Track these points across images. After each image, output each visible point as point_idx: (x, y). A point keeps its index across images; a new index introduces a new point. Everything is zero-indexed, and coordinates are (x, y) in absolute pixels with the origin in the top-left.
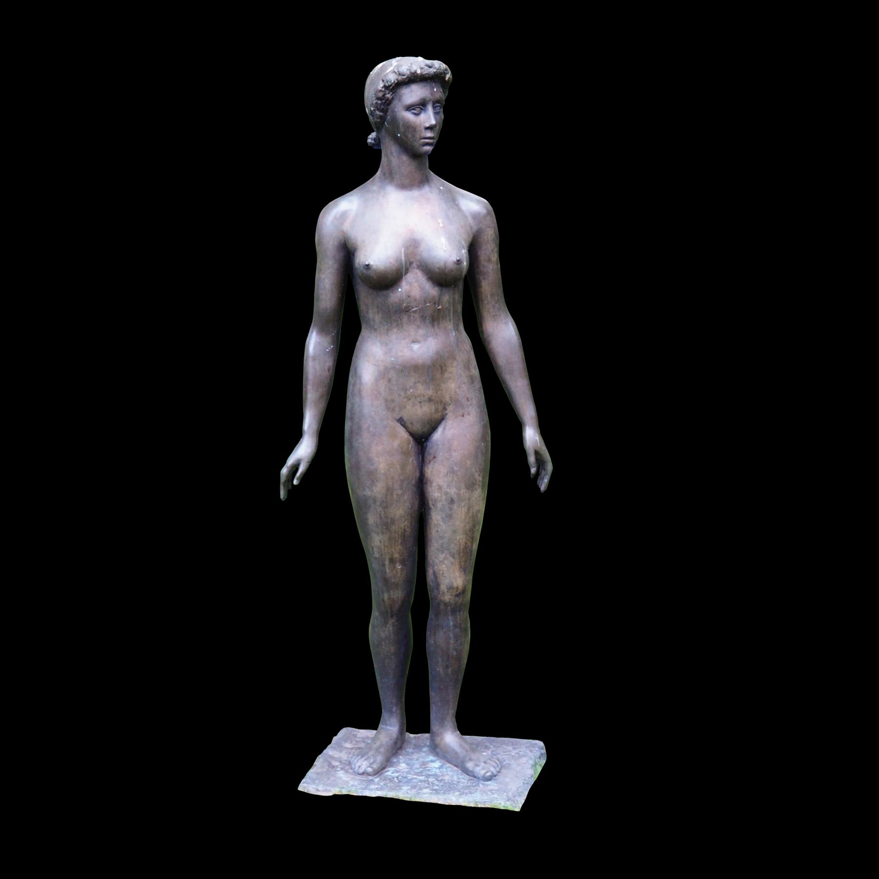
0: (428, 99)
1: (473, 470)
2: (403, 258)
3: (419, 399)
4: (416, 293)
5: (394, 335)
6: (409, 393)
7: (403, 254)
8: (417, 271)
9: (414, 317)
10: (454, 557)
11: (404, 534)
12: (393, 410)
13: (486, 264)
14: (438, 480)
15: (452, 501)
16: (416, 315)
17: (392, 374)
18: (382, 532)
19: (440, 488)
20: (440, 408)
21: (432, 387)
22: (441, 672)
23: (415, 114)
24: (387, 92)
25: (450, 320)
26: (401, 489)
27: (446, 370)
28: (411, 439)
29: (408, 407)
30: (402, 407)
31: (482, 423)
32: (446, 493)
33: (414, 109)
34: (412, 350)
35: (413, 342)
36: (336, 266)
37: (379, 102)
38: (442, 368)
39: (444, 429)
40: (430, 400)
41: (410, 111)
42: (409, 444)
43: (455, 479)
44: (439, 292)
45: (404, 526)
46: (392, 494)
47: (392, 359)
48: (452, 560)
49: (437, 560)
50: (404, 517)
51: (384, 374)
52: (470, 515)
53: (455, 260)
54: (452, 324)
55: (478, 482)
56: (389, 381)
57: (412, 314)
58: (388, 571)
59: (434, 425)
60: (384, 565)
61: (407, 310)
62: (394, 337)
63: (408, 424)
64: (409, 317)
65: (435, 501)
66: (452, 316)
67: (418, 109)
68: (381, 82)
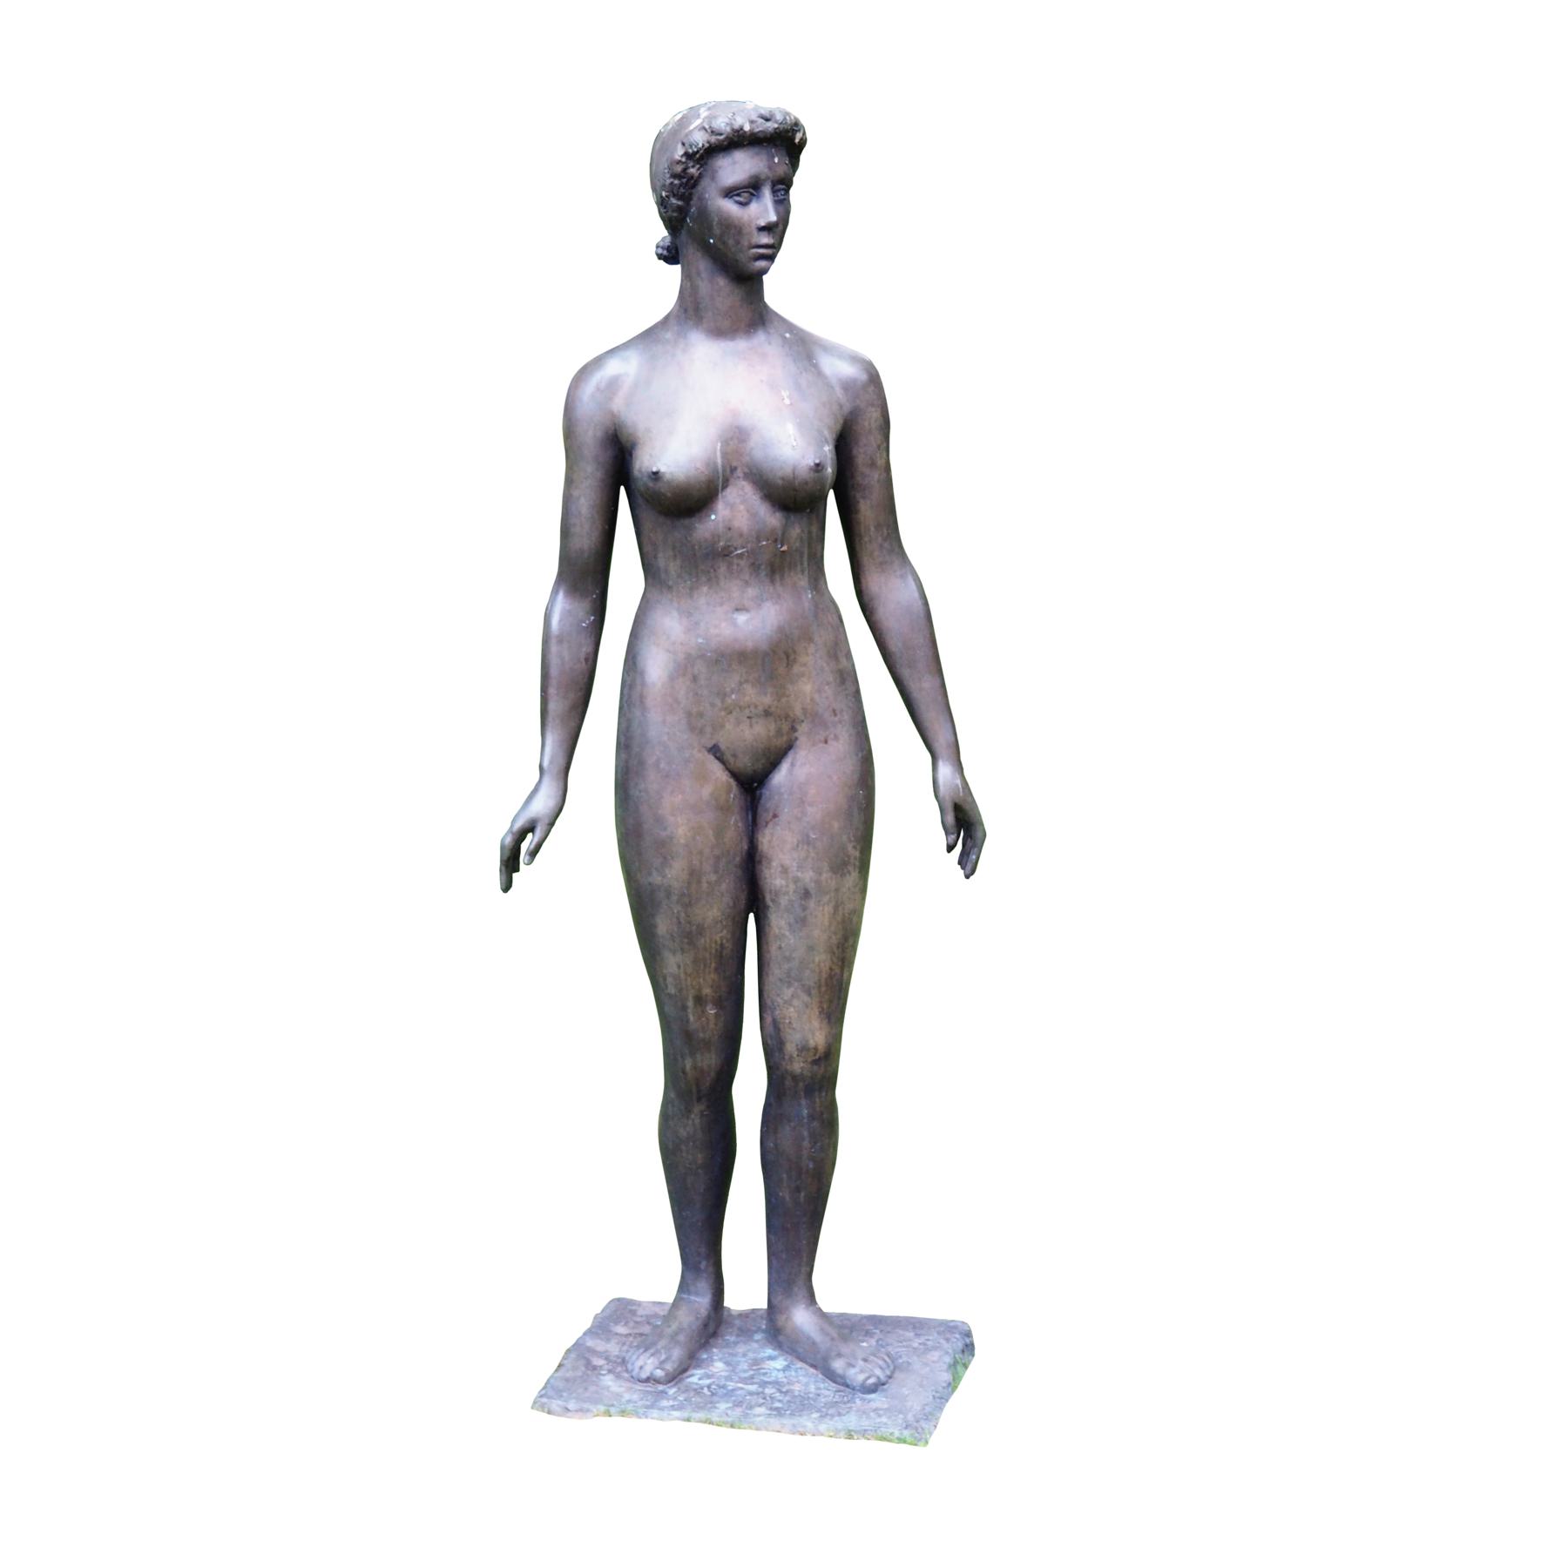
0: (763, 177)
1: (845, 838)
2: (719, 461)
3: (747, 712)
4: (742, 522)
5: (703, 597)
6: (729, 701)
7: (719, 454)
8: (744, 483)
9: (738, 565)
10: (809, 994)
11: (721, 953)
12: (702, 732)
13: (867, 471)
14: (781, 856)
15: (806, 894)
16: (742, 563)
17: (700, 668)
18: (682, 949)
19: (785, 870)
20: (785, 727)
21: (770, 690)
22: (788, 1198)
23: (740, 203)
24: (691, 164)
25: (803, 572)
26: (716, 872)
27: (795, 661)
28: (733, 783)
29: (728, 726)
30: (717, 727)
31: (860, 755)
32: (796, 880)
33: (738, 195)
34: (734, 624)
35: (737, 610)
36: (599, 475)
37: (676, 182)
38: (788, 657)
39: (793, 765)
40: (767, 713)
41: (731, 197)
42: (729, 792)
43: (812, 855)
44: (784, 521)
45: (721, 938)
46: (699, 882)
47: (700, 640)
48: (806, 998)
49: (779, 1000)
50: (721, 922)
51: (685, 667)
52: (839, 918)
53: (812, 464)
54: (806, 579)
55: (852, 860)
56: (695, 679)
57: (735, 561)
58: (691, 1018)
59: (774, 758)
60: (684, 1008)
61: (726, 553)
62: (702, 601)
63: (728, 756)
64: (730, 565)
65: (777, 894)
66: (806, 564)
67: (746, 195)
68: (680, 146)
